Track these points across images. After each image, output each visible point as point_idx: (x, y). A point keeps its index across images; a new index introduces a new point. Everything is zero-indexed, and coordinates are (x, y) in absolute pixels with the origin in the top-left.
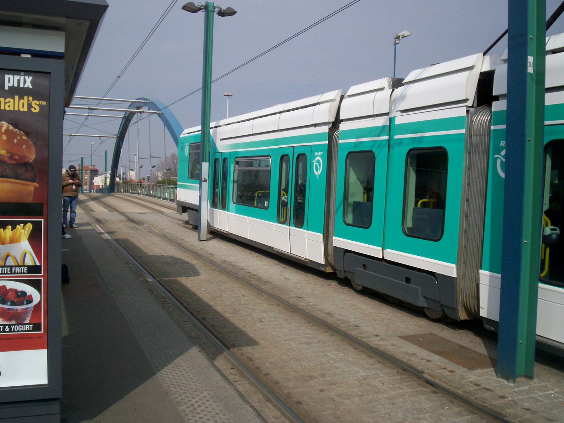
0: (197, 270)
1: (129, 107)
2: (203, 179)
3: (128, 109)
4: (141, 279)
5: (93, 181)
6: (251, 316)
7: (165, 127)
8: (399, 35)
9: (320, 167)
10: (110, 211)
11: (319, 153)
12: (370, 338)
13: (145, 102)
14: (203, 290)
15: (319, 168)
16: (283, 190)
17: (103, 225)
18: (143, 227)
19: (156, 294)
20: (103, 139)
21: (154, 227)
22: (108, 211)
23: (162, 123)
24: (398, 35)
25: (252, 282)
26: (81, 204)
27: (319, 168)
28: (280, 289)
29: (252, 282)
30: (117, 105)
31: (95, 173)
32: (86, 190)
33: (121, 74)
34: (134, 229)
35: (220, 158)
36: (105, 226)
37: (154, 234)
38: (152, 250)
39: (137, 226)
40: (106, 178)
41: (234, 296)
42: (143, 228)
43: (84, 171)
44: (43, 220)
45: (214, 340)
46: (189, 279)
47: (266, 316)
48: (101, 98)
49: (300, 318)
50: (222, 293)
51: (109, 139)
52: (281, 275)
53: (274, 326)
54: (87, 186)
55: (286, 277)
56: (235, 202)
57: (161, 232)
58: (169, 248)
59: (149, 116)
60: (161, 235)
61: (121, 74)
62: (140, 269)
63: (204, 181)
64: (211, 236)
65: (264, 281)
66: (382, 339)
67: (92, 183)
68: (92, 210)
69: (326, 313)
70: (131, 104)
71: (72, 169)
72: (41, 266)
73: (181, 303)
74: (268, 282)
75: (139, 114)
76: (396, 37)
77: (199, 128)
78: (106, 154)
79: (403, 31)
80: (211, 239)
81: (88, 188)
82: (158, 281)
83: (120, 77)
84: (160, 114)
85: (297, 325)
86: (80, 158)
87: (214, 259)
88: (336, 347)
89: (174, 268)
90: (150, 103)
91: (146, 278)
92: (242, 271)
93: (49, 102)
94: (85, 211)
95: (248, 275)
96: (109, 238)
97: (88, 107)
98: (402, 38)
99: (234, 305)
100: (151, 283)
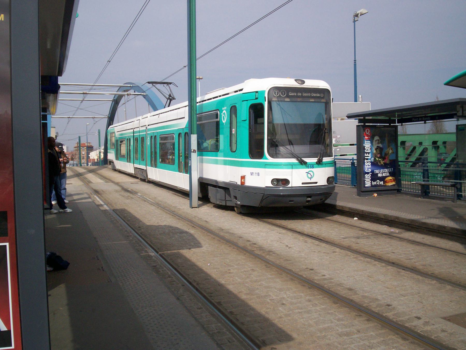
0: (197, 240)
2: (192, 150)
3: (117, 92)
4: (144, 254)
5: (89, 155)
6: (269, 298)
7: (149, 105)
8: (357, 13)
10: (106, 182)
12: (412, 322)
13: (131, 86)
14: (209, 264)
17: (101, 195)
18: (137, 196)
19: (162, 272)
20: (96, 120)
21: (146, 195)
22: (103, 182)
23: (147, 103)
24: (356, 13)
25: (255, 252)
26: (81, 177)
28: (287, 260)
29: (255, 252)
30: (106, 89)
31: (90, 149)
32: (84, 163)
33: (111, 59)
34: (129, 199)
36: (102, 197)
37: (148, 202)
38: (149, 219)
39: (131, 195)
40: (100, 152)
41: (243, 270)
42: (137, 197)
43: (81, 148)
44: (7, 244)
45: (238, 334)
46: (191, 252)
47: (285, 296)
48: (93, 84)
49: (323, 297)
50: (230, 268)
51: (101, 119)
52: (281, 242)
53: (300, 311)
54: (85, 160)
55: (287, 244)
57: (154, 201)
58: (164, 216)
59: (135, 97)
60: (154, 204)
61: (111, 59)
62: (141, 242)
63: (193, 152)
64: (201, 202)
65: (267, 250)
66: (426, 323)
67: (88, 157)
68: (90, 182)
69: (346, 288)
70: (119, 89)
71: (60, 146)
72: (9, 331)
73: (190, 283)
74: (272, 252)
75: (126, 96)
76: (354, 15)
77: (186, 103)
78: (99, 133)
79: (361, 9)
80: (202, 206)
81: (85, 162)
82: (160, 255)
83: (110, 62)
84: (145, 95)
85: (323, 307)
86: (78, 137)
88: (382, 339)
89: (173, 238)
90: (136, 86)
91: (148, 252)
92: (241, 239)
93: (10, 15)
94: (83, 182)
95: (248, 243)
96: (107, 208)
97: (82, 92)
98: (361, 15)
99: (246, 283)
100: (154, 258)
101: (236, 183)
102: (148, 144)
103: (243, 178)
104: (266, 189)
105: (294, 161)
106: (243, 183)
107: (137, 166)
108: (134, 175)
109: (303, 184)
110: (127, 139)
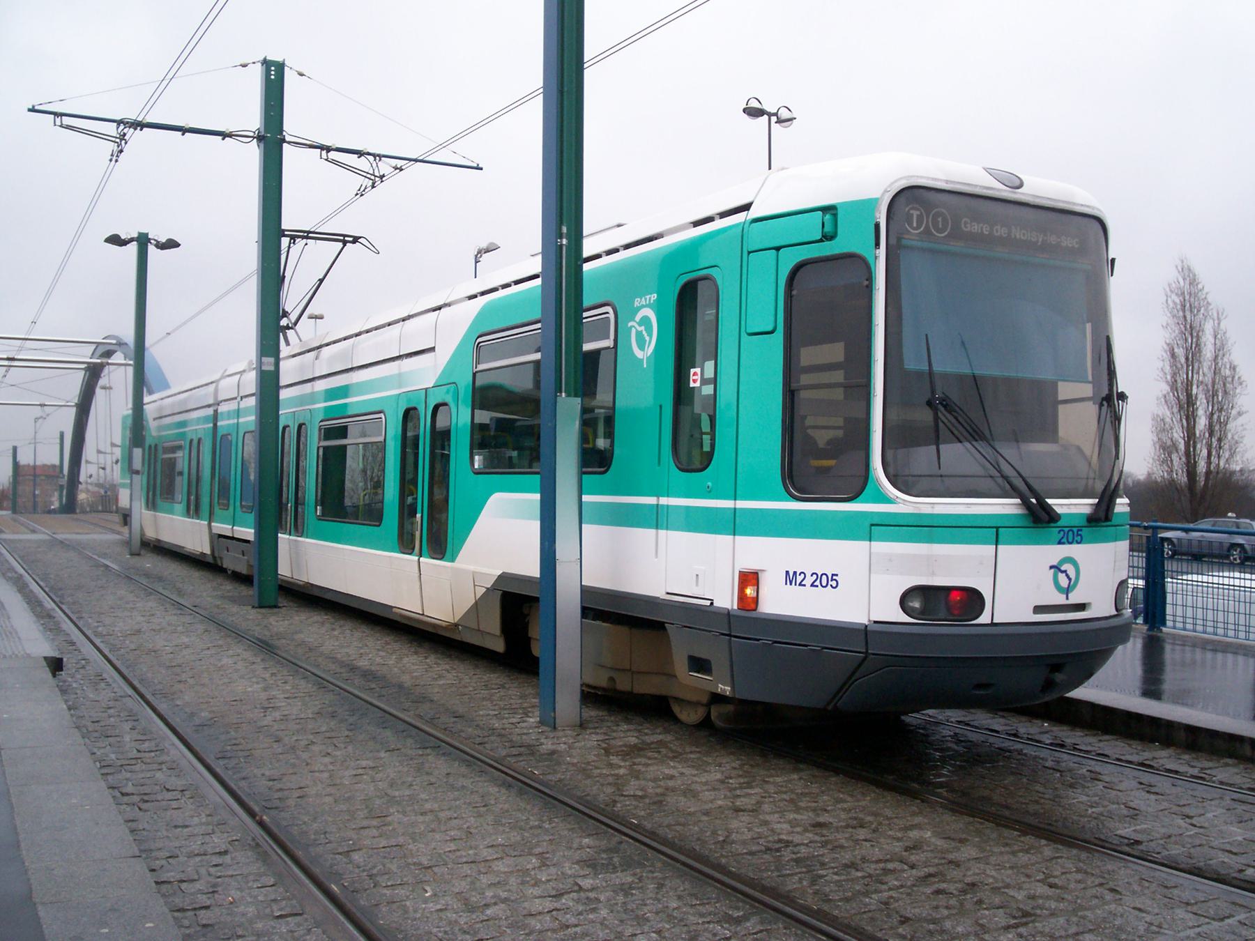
1: (93, 354)
9: (650, 335)
11: (648, 297)
15: (647, 338)
16: (408, 481)
27: (647, 338)
35: (291, 424)
51: (443, 146)
56: (378, 523)
87: (814, 788)
101: (708, 603)
102: (252, 478)
103: (749, 578)
104: (738, 617)
105: (1005, 507)
106: (748, 604)
107: (221, 527)
108: (210, 560)
109: (1038, 609)
110: (191, 441)
